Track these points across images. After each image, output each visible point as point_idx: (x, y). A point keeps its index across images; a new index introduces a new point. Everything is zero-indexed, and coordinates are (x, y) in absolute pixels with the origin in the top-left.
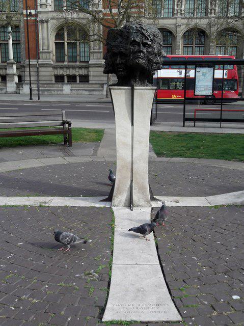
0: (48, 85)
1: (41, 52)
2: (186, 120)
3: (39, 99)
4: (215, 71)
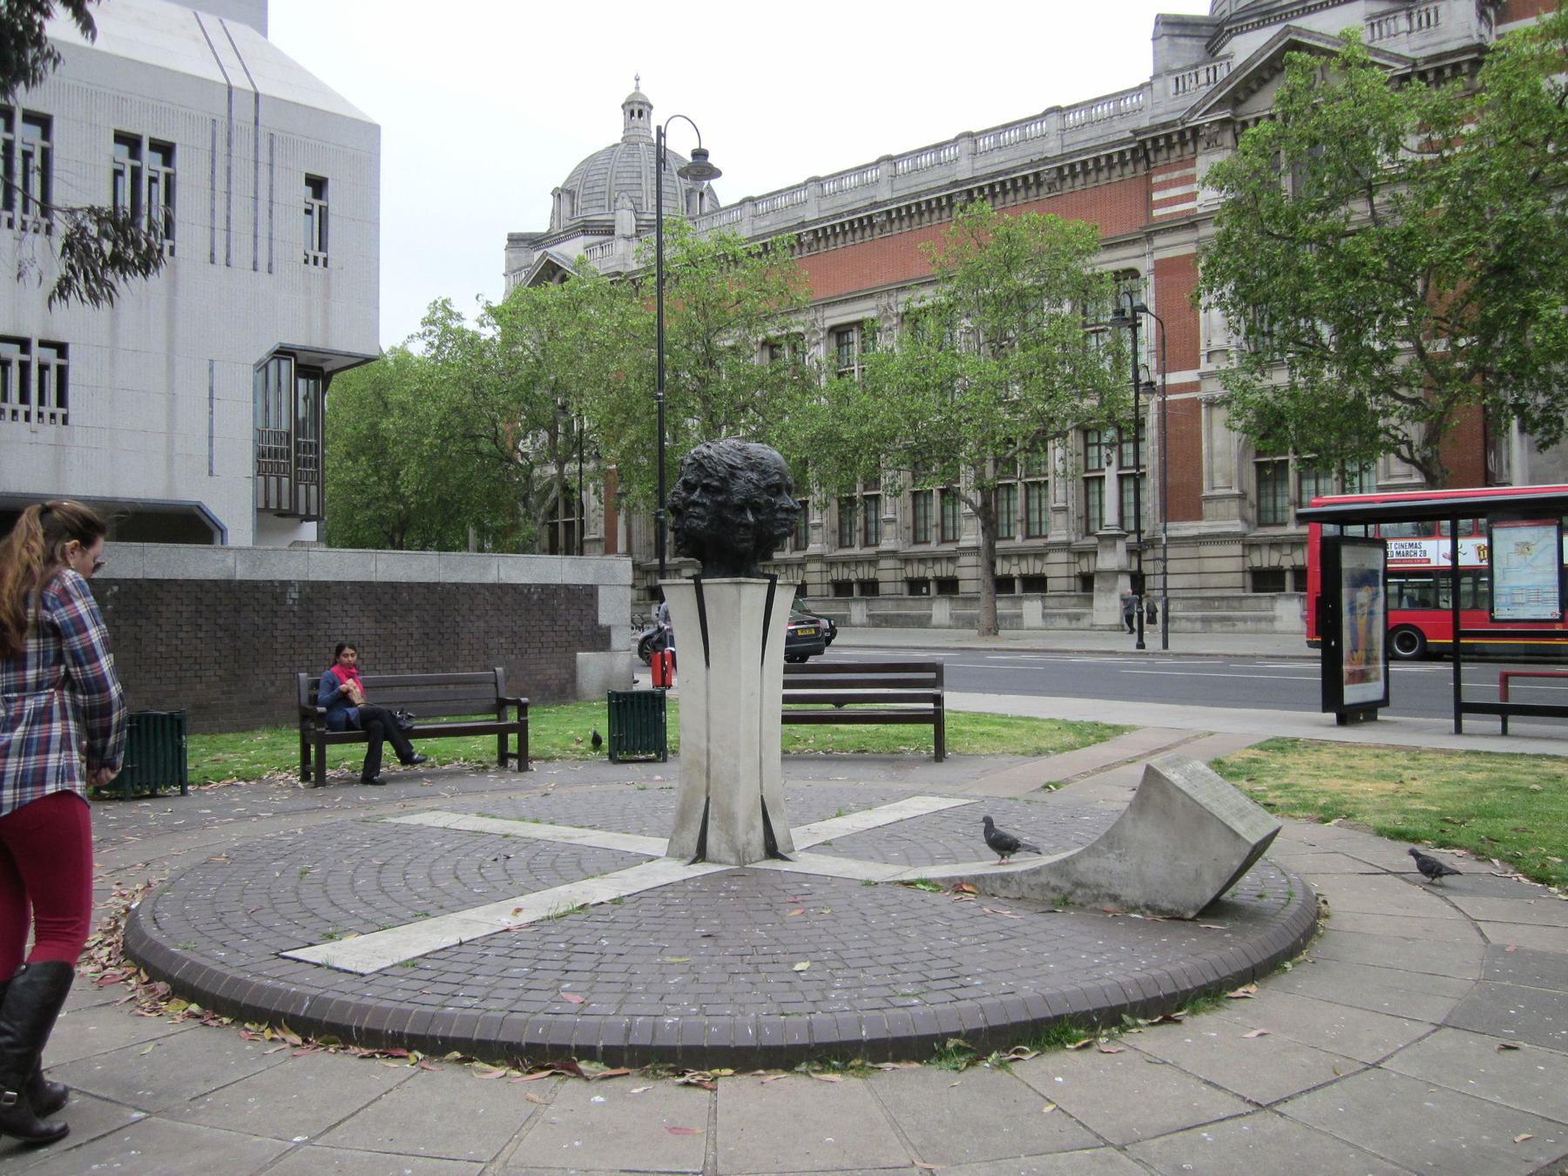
0: (1224, 603)
1: (1208, 499)
2: (1462, 709)
3: (1165, 646)
4: (1460, 542)
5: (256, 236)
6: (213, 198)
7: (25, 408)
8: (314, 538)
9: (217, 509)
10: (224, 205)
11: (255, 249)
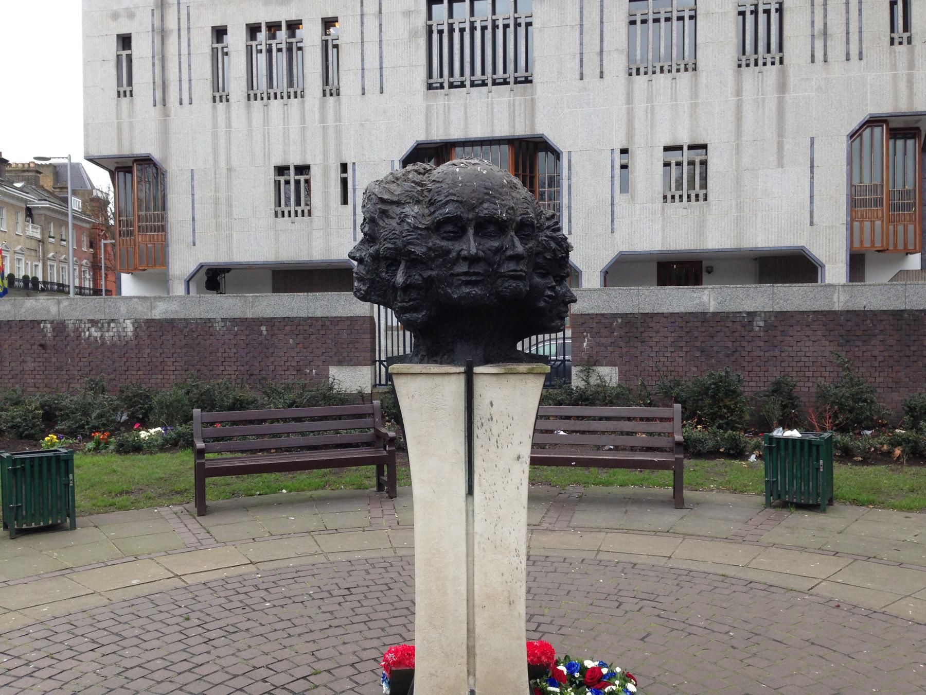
5: (848, 33)
6: (813, 12)
8: (918, 266)
9: (817, 251)
10: (822, 15)
11: (848, 43)
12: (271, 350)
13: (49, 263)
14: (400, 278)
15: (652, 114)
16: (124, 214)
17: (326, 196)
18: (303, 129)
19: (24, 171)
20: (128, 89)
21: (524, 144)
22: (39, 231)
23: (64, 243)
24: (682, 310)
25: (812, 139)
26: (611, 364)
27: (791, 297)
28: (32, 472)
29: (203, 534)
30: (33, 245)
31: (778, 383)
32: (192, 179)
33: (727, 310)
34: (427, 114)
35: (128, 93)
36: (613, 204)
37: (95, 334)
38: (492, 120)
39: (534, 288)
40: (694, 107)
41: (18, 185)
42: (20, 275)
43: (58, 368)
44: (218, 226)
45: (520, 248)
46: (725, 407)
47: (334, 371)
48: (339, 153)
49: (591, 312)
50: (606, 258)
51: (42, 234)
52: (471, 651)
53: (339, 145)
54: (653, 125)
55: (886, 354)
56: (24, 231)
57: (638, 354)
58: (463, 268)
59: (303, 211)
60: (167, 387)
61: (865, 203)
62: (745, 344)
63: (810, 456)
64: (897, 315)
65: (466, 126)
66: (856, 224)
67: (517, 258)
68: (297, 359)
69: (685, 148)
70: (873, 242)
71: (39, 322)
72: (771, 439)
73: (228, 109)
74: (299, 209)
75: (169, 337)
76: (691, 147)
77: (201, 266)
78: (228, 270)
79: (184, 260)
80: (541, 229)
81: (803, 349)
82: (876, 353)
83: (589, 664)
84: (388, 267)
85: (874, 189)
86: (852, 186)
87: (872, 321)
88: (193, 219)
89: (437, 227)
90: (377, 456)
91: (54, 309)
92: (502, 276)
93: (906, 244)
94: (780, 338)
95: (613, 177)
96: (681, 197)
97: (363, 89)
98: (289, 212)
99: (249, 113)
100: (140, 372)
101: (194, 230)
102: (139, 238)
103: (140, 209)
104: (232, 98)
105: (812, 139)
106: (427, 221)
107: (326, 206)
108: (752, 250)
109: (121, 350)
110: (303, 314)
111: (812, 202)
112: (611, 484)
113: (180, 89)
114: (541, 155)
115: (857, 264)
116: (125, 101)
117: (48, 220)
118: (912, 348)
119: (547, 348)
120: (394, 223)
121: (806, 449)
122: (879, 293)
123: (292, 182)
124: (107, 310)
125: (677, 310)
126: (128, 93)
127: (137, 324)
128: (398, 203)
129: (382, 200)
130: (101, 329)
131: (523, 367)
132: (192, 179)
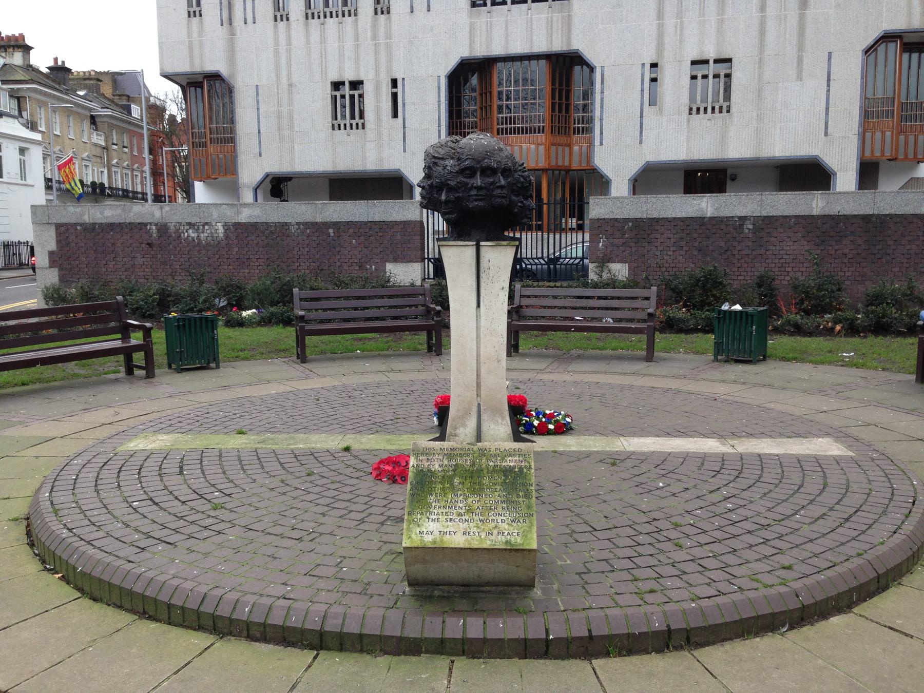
7: (344, 122)
9: (830, 160)
12: (338, 249)
13: (114, 169)
14: (443, 197)
15: (681, 30)
16: (196, 126)
17: (378, 109)
18: (357, 47)
19: (85, 79)
20: (197, 9)
21: (561, 59)
22: (103, 138)
23: (126, 150)
24: (684, 215)
25: (830, 54)
26: (621, 261)
27: (814, 203)
28: (190, 329)
29: (308, 372)
30: (98, 151)
31: (761, 277)
32: (257, 94)
33: (722, 215)
34: (471, 30)
35: (197, 13)
36: (642, 117)
37: (193, 235)
38: (531, 36)
39: (511, 202)
40: (721, 22)
41: (81, 93)
42: (88, 180)
43: (163, 263)
44: (282, 139)
45: (503, 182)
46: (714, 296)
47: (389, 267)
48: (389, 69)
49: (606, 217)
50: (634, 167)
51: (106, 141)
52: (478, 385)
53: (389, 61)
54: (681, 40)
55: (855, 252)
56: (90, 138)
57: (645, 252)
58: (474, 192)
59: (357, 124)
60: (254, 278)
61: (877, 114)
62: (736, 244)
63: (747, 323)
64: (866, 218)
65: (507, 42)
66: (868, 135)
67: (502, 187)
68: (360, 256)
69: (711, 62)
70: (883, 151)
71: (146, 225)
72: (720, 311)
73: (289, 26)
74: (354, 122)
75: (253, 238)
76: (716, 61)
77: (267, 175)
78: (290, 179)
79: (251, 171)
80: (516, 171)
81: (785, 248)
82: (846, 251)
83: (548, 412)
84: (438, 191)
85: (883, 101)
86: (866, 98)
87: (845, 224)
88: (259, 132)
89: (462, 171)
90: (426, 322)
91: (157, 214)
92: (494, 196)
93: (915, 154)
94: (766, 239)
95: (642, 90)
96: (706, 109)
97: (412, 7)
98: (345, 125)
99: (307, 31)
100: (230, 267)
101: (260, 142)
102: (211, 149)
103: (211, 122)
104: (292, 17)
105: (830, 54)
106: (457, 169)
107: (379, 119)
108: (769, 159)
109: (215, 247)
110: (364, 219)
111: (827, 114)
112: (606, 349)
113: (245, 9)
114: (577, 68)
115: (868, 173)
116: (195, 20)
117: (111, 127)
118: (878, 247)
119: (574, 251)
120: (440, 169)
121: (744, 318)
122: (891, 198)
123: (347, 97)
124: (202, 215)
125: (679, 215)
126: (197, 13)
127: (225, 225)
128: (442, 159)
129: (434, 157)
130: (197, 230)
131: (505, 243)
132: (257, 94)
